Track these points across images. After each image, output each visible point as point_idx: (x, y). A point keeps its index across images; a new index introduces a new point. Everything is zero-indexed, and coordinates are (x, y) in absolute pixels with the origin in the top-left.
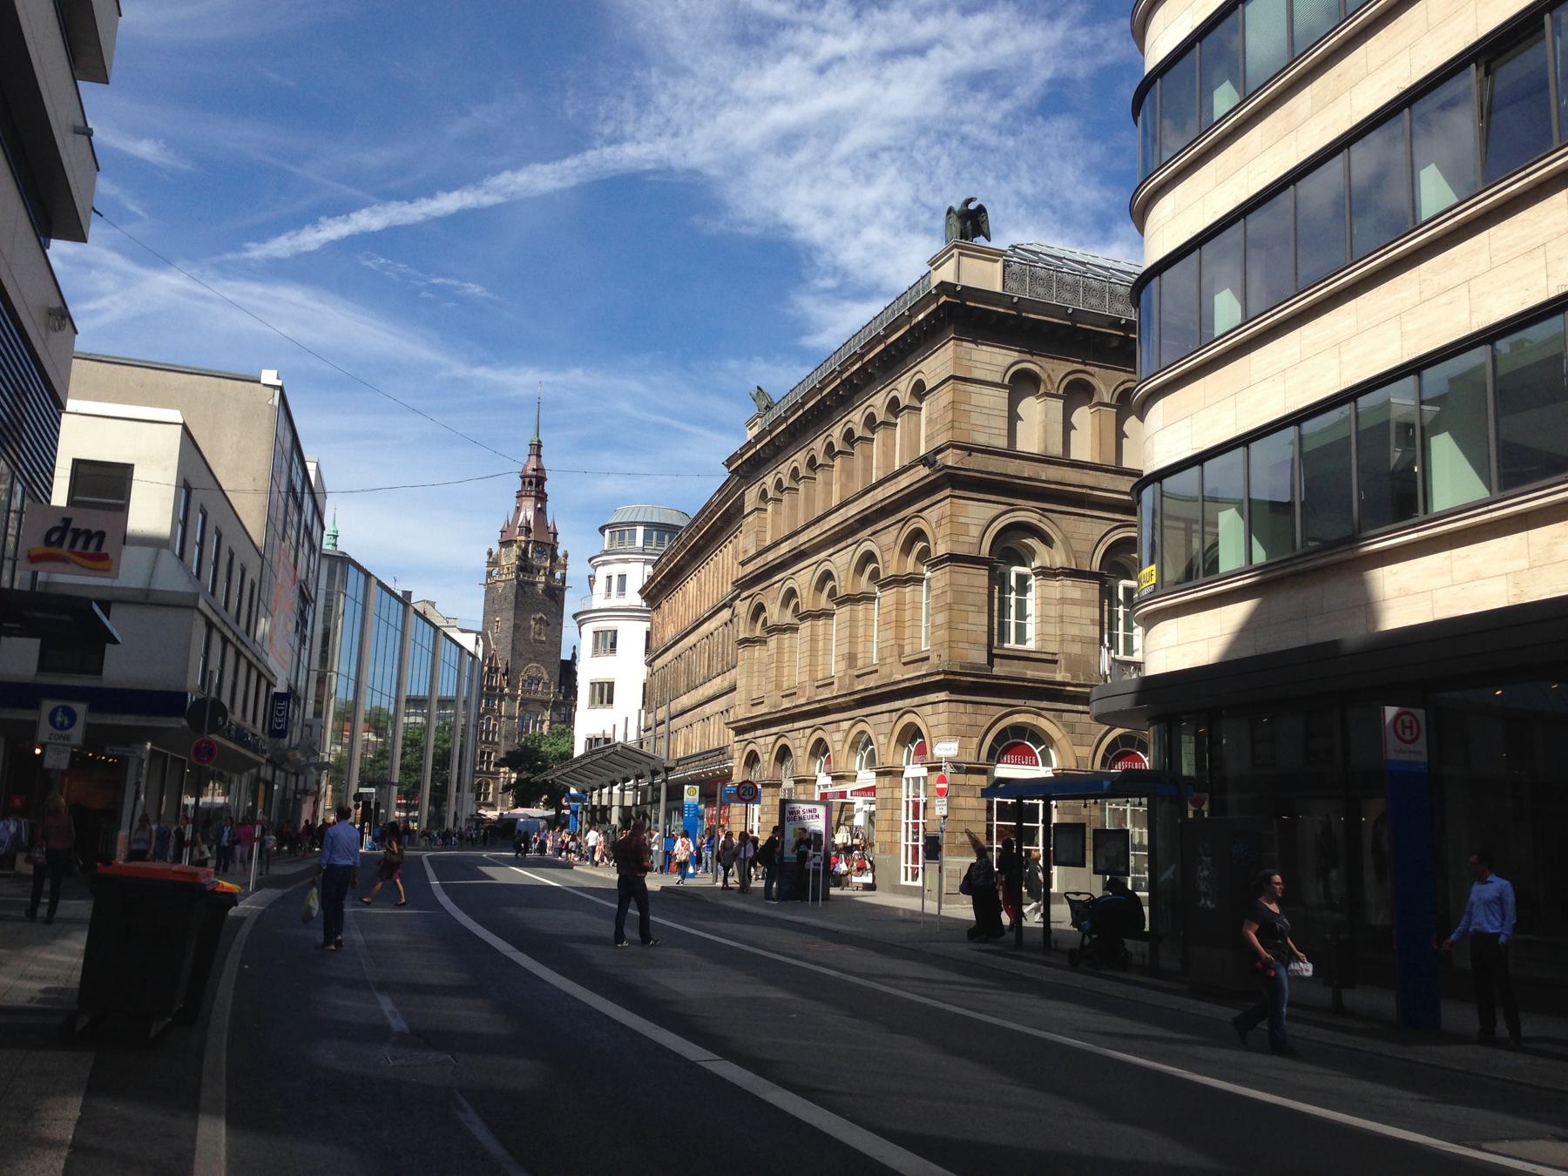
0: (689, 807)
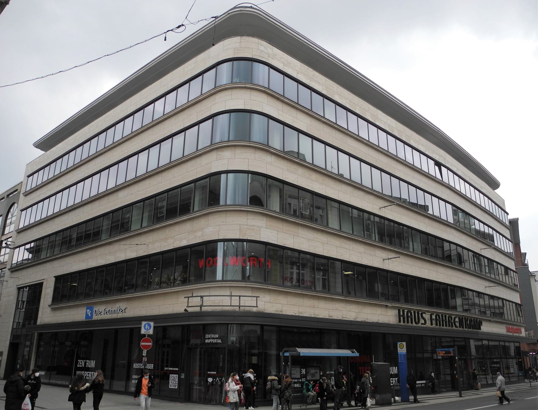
0: (400, 356)
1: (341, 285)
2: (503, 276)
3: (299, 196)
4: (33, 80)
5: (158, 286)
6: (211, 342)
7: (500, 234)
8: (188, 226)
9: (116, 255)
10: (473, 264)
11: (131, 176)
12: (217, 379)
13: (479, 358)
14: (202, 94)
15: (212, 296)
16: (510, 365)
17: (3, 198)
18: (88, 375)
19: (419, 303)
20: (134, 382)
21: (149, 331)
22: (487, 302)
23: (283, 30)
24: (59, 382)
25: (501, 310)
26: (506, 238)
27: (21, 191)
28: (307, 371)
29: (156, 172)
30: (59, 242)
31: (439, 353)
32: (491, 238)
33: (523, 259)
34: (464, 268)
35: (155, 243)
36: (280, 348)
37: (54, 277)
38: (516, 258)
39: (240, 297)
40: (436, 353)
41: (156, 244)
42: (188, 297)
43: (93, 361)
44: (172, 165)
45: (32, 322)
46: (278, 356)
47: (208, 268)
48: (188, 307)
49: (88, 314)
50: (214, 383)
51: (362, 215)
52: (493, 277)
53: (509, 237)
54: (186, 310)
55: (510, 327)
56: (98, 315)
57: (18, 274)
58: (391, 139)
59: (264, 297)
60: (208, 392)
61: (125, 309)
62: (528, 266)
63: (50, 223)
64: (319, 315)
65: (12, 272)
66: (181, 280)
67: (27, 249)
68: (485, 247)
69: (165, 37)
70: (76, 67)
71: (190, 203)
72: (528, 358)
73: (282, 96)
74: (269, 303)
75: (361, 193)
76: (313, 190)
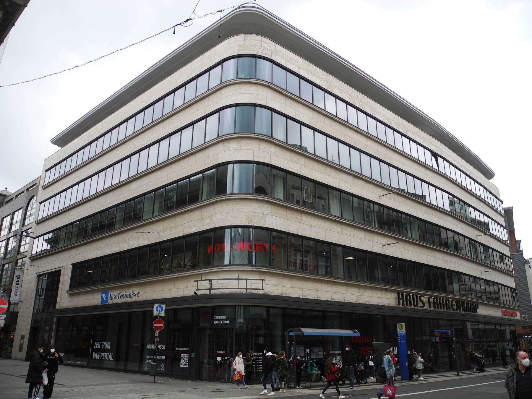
0: (400, 337)
1: (342, 271)
2: (498, 262)
3: (301, 187)
4: (50, 75)
5: (169, 271)
6: (219, 323)
7: (495, 221)
8: (196, 215)
9: (129, 243)
10: (469, 251)
11: (143, 168)
12: (232, 358)
13: (476, 341)
14: (209, 89)
15: (220, 279)
16: (506, 347)
17: (23, 192)
18: (104, 356)
19: (417, 287)
20: (147, 362)
21: (161, 313)
22: (483, 287)
23: (287, 29)
24: (77, 363)
25: (497, 296)
26: (501, 225)
27: (40, 185)
28: (311, 350)
29: (166, 163)
30: (76, 233)
31: (437, 334)
32: (487, 226)
33: (517, 245)
34: (461, 253)
35: (165, 231)
36: (285, 328)
37: (71, 264)
38: (511, 245)
39: (246, 280)
40: (434, 336)
41: (166, 232)
42: (198, 281)
43: (108, 343)
44: (181, 157)
45: (52, 307)
46: (283, 336)
47: (216, 254)
48: (197, 290)
49: (103, 299)
50: (223, 362)
51: (362, 203)
52: (489, 263)
53: (504, 225)
54: (195, 293)
55: (506, 310)
56: (113, 299)
57: (38, 263)
58: (390, 131)
59: (269, 281)
60: (217, 370)
61: (138, 293)
62: (522, 253)
63: (67, 214)
64: (322, 297)
65: (32, 260)
66: (190, 266)
67: (46, 240)
68: (480, 233)
69: (174, 31)
70: (91, 61)
71: (199, 194)
72: (523, 340)
73: (284, 91)
74: (275, 286)
75: (361, 182)
76: (315, 179)
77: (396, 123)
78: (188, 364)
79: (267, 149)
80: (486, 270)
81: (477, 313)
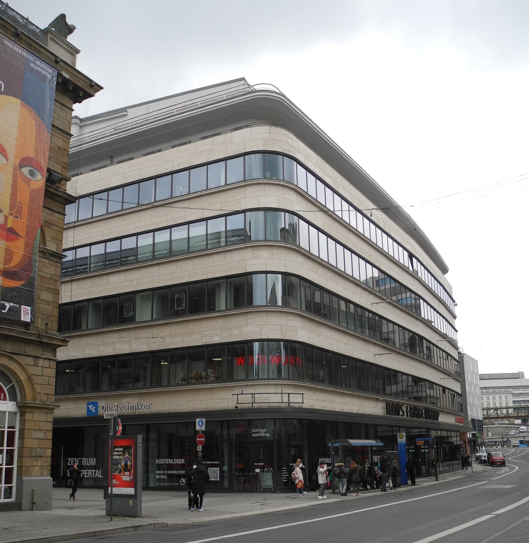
0: (400, 445)
12: (265, 470)
39: (289, 395)
41: (175, 339)
49: (91, 410)
77: (383, 222)
78: (219, 477)
79: (296, 259)
80: (445, 377)
81: (438, 421)
